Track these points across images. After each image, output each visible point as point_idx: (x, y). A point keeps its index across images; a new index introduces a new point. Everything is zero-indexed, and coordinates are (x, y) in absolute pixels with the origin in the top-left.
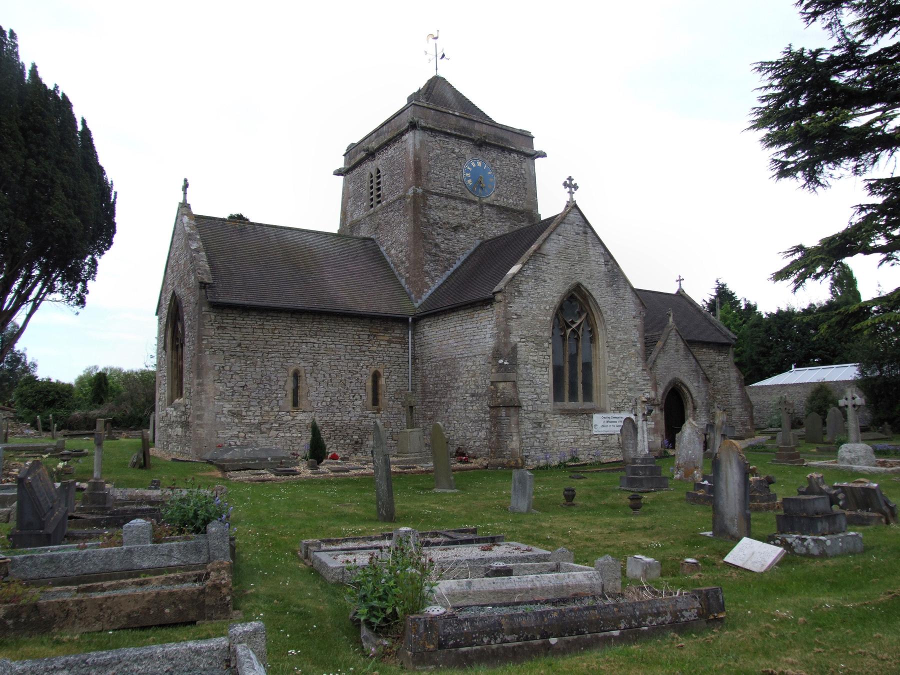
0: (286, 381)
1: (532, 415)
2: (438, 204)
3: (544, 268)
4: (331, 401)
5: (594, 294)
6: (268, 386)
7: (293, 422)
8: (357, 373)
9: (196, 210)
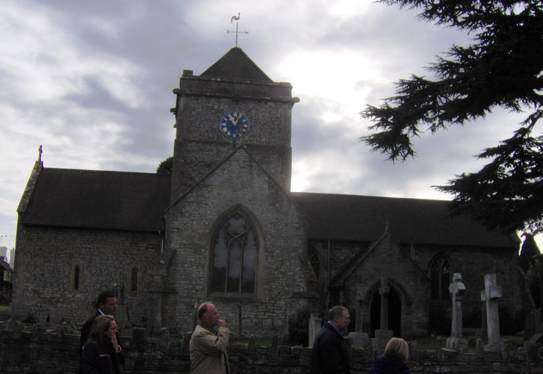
0: (70, 273)
1: (187, 300)
2: (195, 149)
3: (206, 195)
4: (101, 286)
5: (255, 212)
6: (57, 275)
7: (73, 299)
8: (120, 268)
9: (46, 166)
